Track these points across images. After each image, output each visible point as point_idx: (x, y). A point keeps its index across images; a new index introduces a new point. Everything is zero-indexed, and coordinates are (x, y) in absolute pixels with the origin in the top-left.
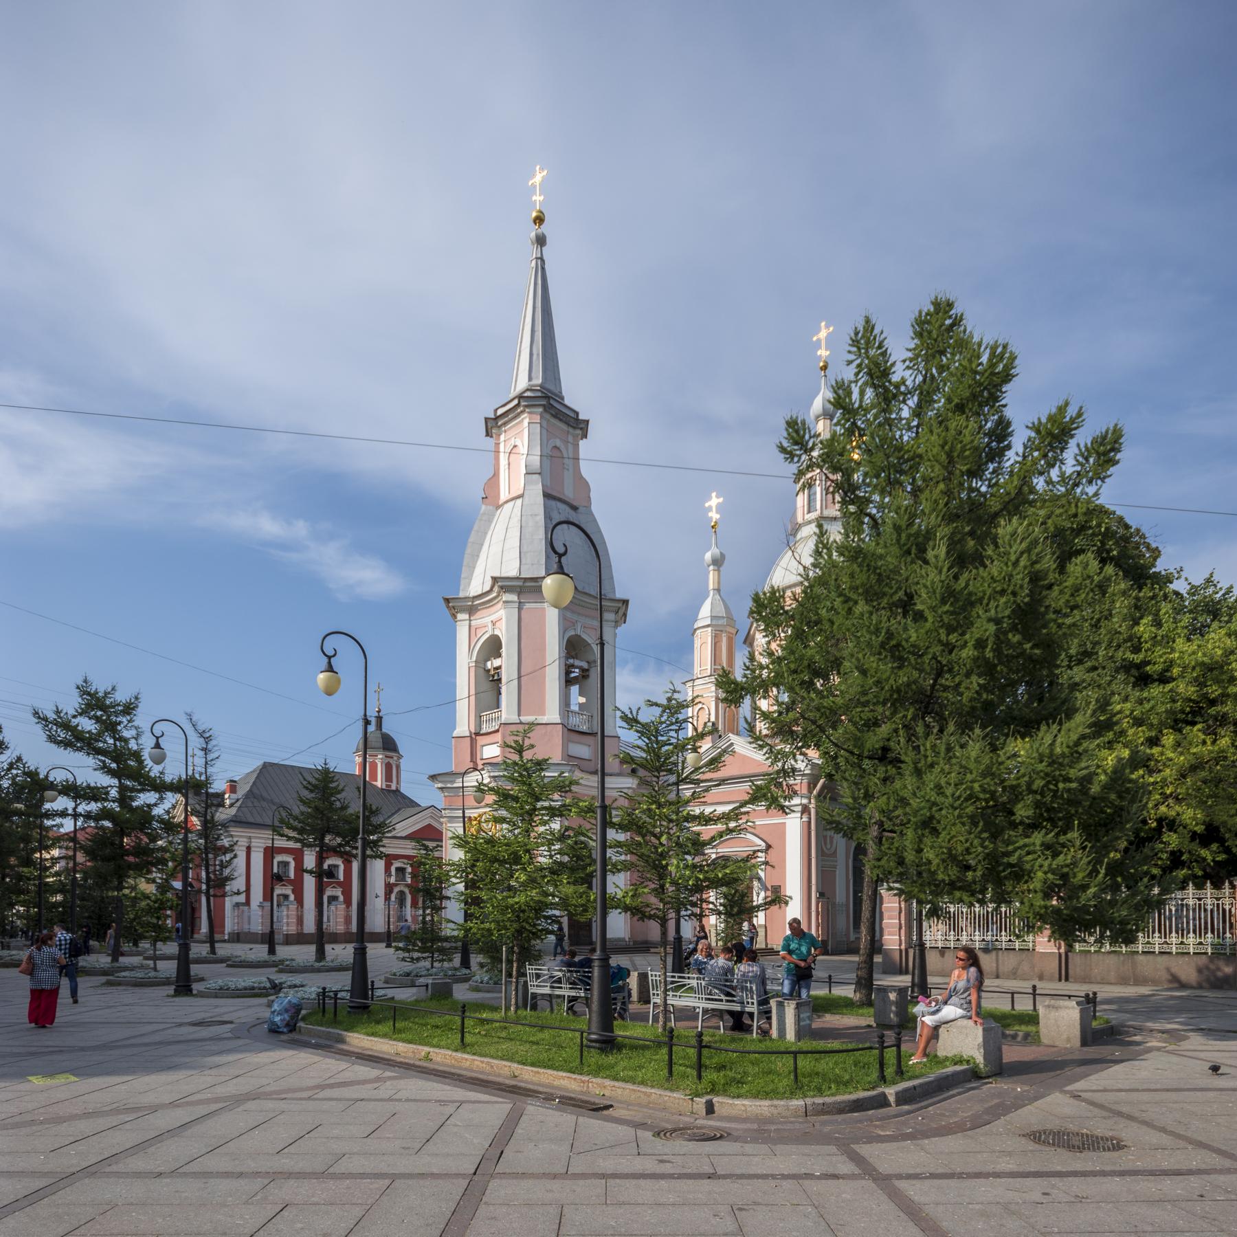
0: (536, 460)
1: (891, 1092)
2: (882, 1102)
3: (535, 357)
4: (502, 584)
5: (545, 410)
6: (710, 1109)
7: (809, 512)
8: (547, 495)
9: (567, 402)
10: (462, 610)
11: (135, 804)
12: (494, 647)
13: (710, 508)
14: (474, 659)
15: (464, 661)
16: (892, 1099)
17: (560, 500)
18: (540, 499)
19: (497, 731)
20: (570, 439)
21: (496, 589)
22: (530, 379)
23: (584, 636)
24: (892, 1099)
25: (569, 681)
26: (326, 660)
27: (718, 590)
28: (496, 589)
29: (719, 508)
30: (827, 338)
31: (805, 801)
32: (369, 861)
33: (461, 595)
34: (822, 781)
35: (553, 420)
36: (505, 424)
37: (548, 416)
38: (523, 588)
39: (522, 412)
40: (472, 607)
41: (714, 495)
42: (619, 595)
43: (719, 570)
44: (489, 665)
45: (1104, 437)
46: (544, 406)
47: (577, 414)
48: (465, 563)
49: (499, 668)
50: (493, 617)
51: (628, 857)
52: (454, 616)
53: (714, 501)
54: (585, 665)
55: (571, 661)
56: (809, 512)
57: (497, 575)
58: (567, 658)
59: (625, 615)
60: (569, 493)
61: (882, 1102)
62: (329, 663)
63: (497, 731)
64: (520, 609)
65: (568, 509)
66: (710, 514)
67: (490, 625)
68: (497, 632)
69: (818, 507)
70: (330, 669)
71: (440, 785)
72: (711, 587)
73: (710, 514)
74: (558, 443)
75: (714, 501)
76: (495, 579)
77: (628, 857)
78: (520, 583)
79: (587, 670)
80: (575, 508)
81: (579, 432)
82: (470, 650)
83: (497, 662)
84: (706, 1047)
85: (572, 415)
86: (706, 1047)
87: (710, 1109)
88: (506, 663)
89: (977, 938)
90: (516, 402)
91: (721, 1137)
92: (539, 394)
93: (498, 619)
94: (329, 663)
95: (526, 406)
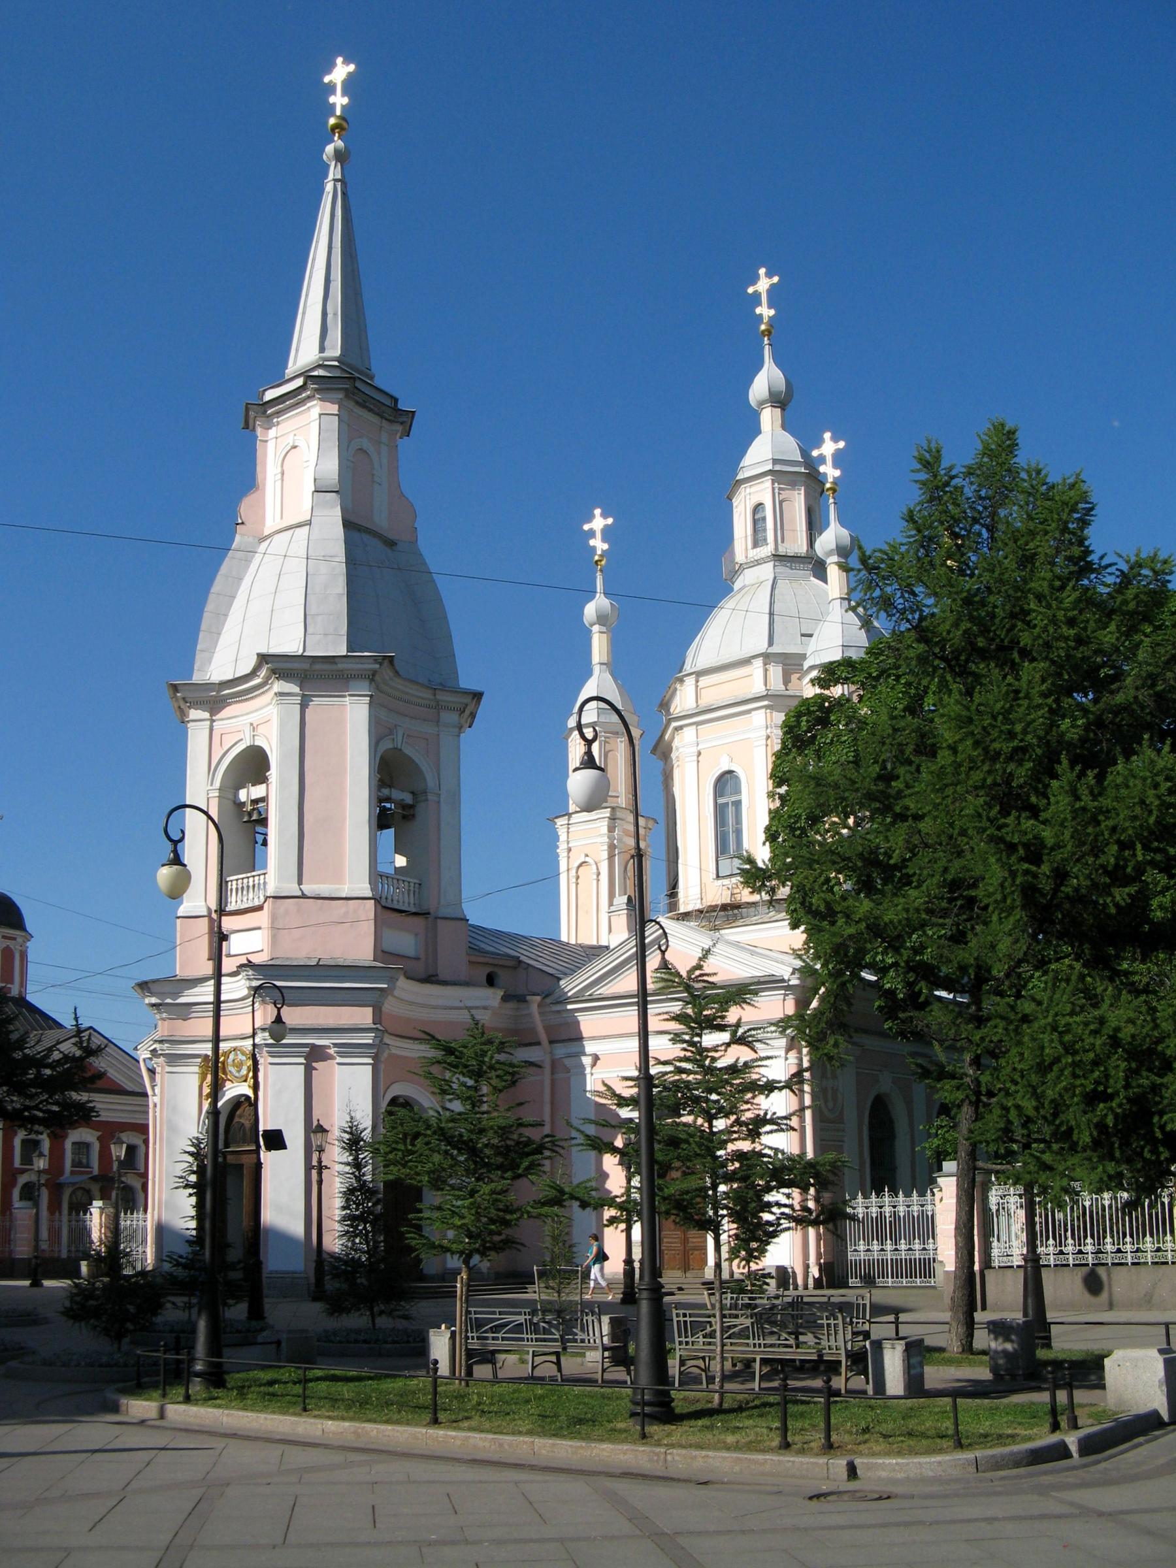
0: (331, 466)
1: (1072, 1440)
2: (1061, 1452)
3: (330, 317)
4: (277, 666)
5: (347, 396)
6: (852, 1471)
7: (756, 545)
8: (348, 524)
9: (377, 382)
10: (198, 704)
12: (254, 765)
13: (592, 534)
14: (217, 784)
15: (201, 786)
16: (1073, 1448)
17: (368, 531)
18: (339, 531)
19: (259, 908)
20: (384, 437)
21: (263, 673)
22: (322, 349)
23: (408, 751)
24: (1073, 1448)
25: (382, 820)
26: (169, 846)
28: (263, 673)
29: (607, 533)
30: (769, 291)
33: (197, 678)
35: (359, 411)
36: (279, 413)
37: (350, 404)
38: (306, 674)
39: (309, 398)
40: (215, 698)
41: (598, 512)
42: (466, 682)
44: (243, 795)
46: (346, 390)
47: (396, 400)
48: (204, 626)
49: (263, 799)
50: (254, 718)
52: (183, 714)
53: (598, 523)
54: (408, 798)
55: (386, 791)
56: (756, 545)
57: (264, 651)
58: (379, 790)
59: (473, 716)
60: (381, 520)
61: (1061, 1452)
62: (175, 852)
63: (259, 908)
64: (304, 706)
65: (379, 545)
66: (592, 542)
67: (248, 729)
70: (177, 860)
71: (154, 1000)
73: (592, 542)
74: (366, 444)
75: (598, 523)
76: (263, 658)
78: (306, 666)
79: (412, 807)
80: (391, 544)
81: (399, 428)
82: (211, 771)
83: (257, 791)
85: (388, 402)
87: (852, 1471)
88: (276, 793)
89: (1070, 1249)
90: (299, 382)
91: (889, 1497)
92: (338, 374)
93: (264, 720)
94: (175, 852)
95: (316, 390)
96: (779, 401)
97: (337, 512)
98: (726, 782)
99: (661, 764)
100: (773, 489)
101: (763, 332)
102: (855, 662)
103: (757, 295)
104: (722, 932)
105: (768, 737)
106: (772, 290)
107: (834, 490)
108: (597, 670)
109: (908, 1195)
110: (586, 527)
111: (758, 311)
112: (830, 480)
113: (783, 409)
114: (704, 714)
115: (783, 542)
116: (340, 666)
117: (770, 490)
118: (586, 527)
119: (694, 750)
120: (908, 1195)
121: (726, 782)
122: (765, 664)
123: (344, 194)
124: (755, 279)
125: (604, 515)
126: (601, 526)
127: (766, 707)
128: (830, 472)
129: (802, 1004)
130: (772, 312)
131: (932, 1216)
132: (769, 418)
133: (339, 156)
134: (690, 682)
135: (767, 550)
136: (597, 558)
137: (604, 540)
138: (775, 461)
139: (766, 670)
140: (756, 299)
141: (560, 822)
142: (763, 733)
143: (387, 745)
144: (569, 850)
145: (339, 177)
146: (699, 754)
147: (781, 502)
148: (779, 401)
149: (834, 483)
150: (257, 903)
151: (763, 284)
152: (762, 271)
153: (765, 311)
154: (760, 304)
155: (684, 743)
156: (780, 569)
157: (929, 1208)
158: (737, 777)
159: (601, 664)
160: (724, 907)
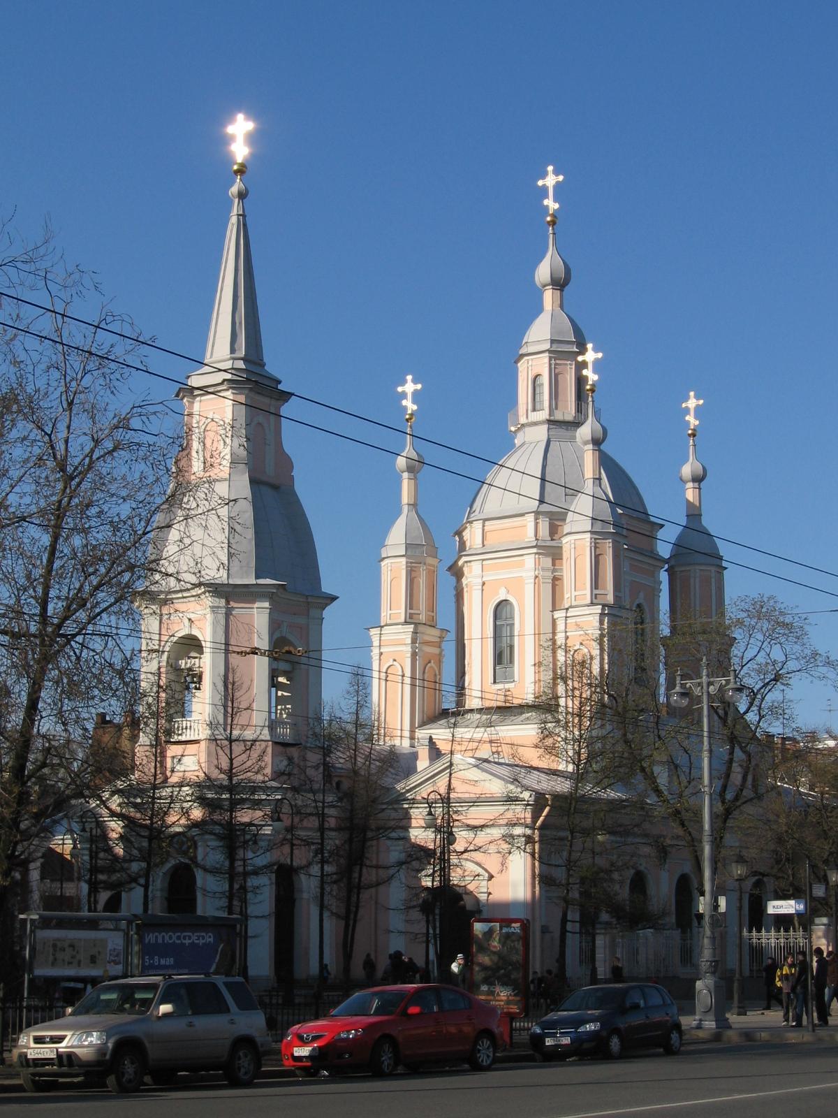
8: (254, 482)
11: (728, 1015)
13: (404, 395)
27: (414, 506)
29: (417, 396)
31: (528, 832)
32: (380, 863)
34: (547, 809)
41: (409, 378)
43: (415, 478)
45: (397, 757)
51: (437, 911)
53: (410, 387)
56: (534, 410)
66: (404, 403)
68: (195, 632)
69: (546, 404)
72: (405, 500)
73: (404, 403)
75: (410, 387)
77: (437, 911)
84: (235, 740)
86: (235, 740)
96: (560, 284)
97: (246, 477)
98: (502, 611)
99: (454, 579)
100: (550, 365)
101: (548, 222)
102: (478, 911)
103: (545, 188)
104: (497, 728)
105: (536, 577)
106: (558, 186)
107: (592, 391)
108: (405, 509)
109: (768, 931)
110: (400, 389)
111: (546, 202)
112: (590, 382)
113: (561, 290)
114: (485, 551)
115: (556, 408)
116: (251, 590)
117: (547, 365)
118: (400, 389)
119: (480, 581)
120: (768, 931)
121: (502, 611)
122: (536, 519)
123: (245, 225)
124: (544, 175)
125: (415, 381)
126: (412, 390)
127: (536, 553)
128: (591, 376)
129: (535, 817)
130: (557, 206)
131: (691, 948)
132: (549, 297)
133: (242, 196)
134: (477, 526)
135: (543, 415)
136: (407, 417)
137: (414, 402)
138: (553, 341)
139: (536, 524)
140: (544, 191)
141: (374, 632)
142: (532, 574)
143: (277, 635)
144: (381, 654)
145: (241, 212)
146: (484, 584)
147: (556, 375)
148: (560, 284)
149: (593, 385)
150: (196, 738)
151: (551, 180)
152: (550, 168)
153: (551, 204)
154: (547, 197)
155: (473, 574)
156: (551, 427)
157: (689, 942)
158: (511, 604)
159: (409, 505)
160: (499, 709)
